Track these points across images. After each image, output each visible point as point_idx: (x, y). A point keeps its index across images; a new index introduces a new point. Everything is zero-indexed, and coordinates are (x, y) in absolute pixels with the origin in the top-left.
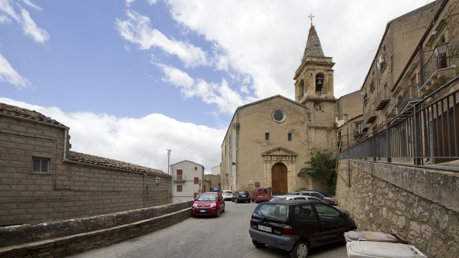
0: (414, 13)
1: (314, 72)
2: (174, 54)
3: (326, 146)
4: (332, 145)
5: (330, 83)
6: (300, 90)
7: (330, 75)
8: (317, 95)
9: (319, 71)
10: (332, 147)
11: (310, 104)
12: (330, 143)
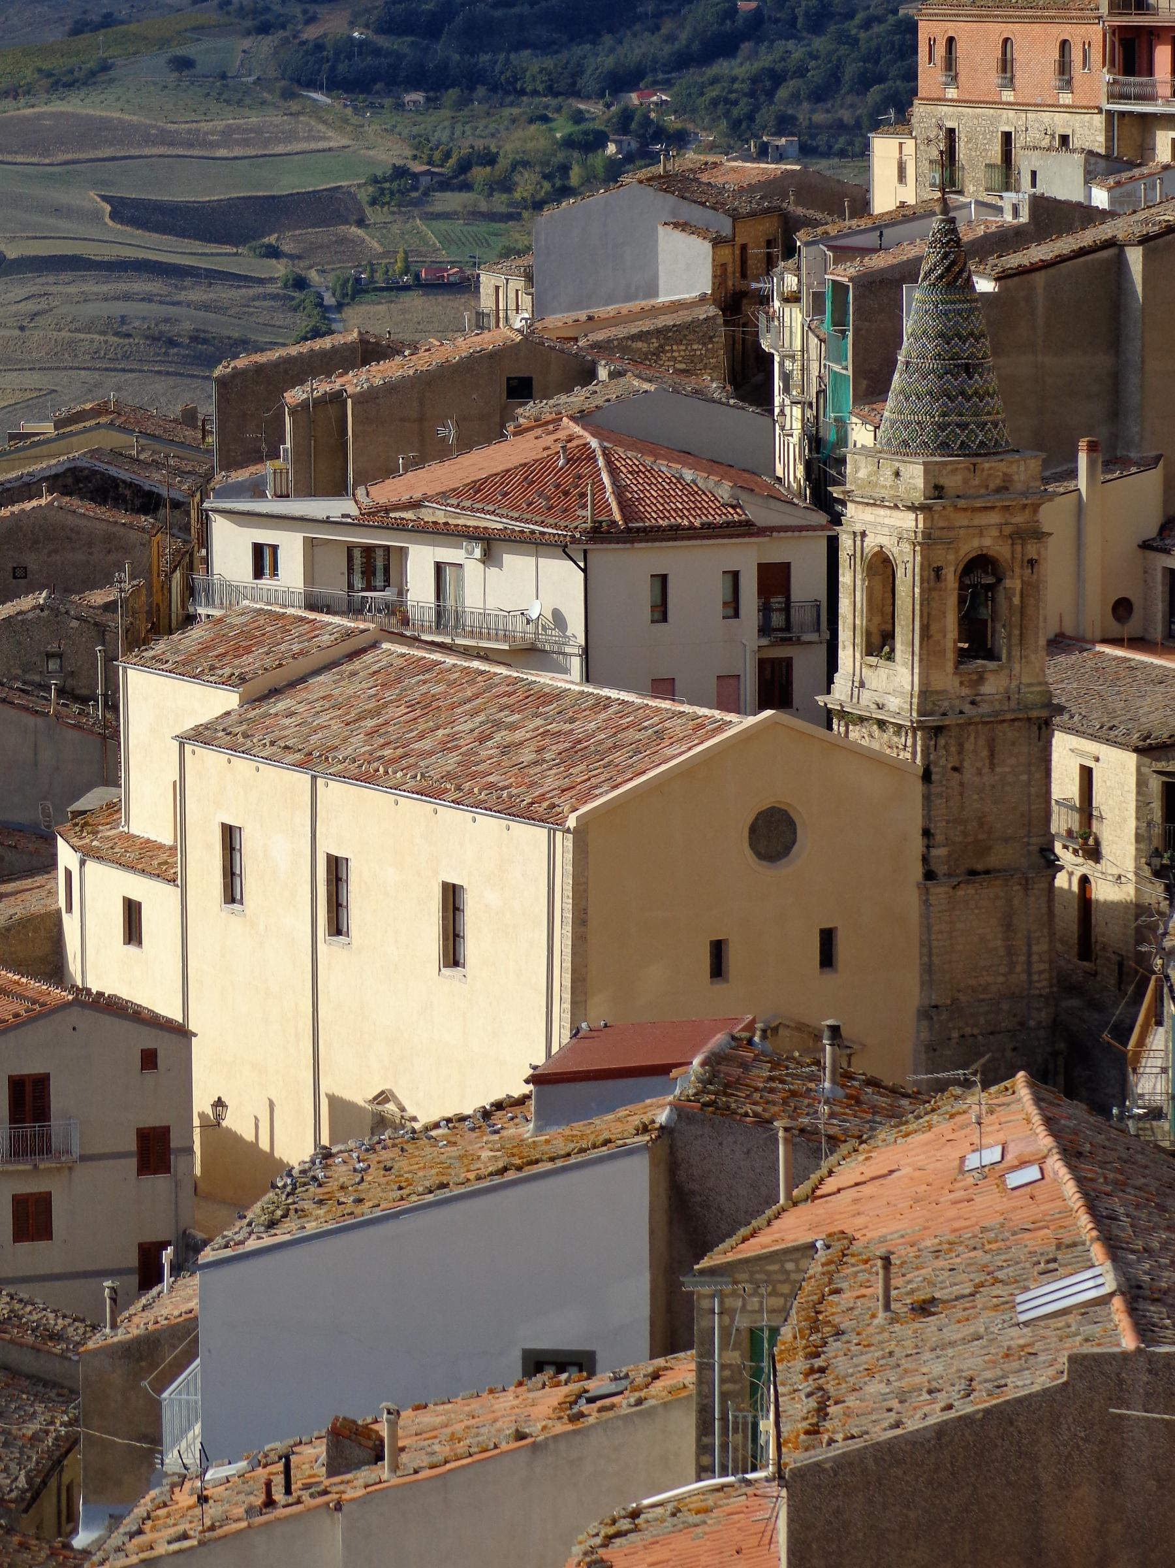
2: (509, 342)
3: (1001, 979)
4: (1029, 973)
7: (1032, 563)
8: (961, 683)
9: (976, 543)
10: (1030, 982)
12: (1022, 959)
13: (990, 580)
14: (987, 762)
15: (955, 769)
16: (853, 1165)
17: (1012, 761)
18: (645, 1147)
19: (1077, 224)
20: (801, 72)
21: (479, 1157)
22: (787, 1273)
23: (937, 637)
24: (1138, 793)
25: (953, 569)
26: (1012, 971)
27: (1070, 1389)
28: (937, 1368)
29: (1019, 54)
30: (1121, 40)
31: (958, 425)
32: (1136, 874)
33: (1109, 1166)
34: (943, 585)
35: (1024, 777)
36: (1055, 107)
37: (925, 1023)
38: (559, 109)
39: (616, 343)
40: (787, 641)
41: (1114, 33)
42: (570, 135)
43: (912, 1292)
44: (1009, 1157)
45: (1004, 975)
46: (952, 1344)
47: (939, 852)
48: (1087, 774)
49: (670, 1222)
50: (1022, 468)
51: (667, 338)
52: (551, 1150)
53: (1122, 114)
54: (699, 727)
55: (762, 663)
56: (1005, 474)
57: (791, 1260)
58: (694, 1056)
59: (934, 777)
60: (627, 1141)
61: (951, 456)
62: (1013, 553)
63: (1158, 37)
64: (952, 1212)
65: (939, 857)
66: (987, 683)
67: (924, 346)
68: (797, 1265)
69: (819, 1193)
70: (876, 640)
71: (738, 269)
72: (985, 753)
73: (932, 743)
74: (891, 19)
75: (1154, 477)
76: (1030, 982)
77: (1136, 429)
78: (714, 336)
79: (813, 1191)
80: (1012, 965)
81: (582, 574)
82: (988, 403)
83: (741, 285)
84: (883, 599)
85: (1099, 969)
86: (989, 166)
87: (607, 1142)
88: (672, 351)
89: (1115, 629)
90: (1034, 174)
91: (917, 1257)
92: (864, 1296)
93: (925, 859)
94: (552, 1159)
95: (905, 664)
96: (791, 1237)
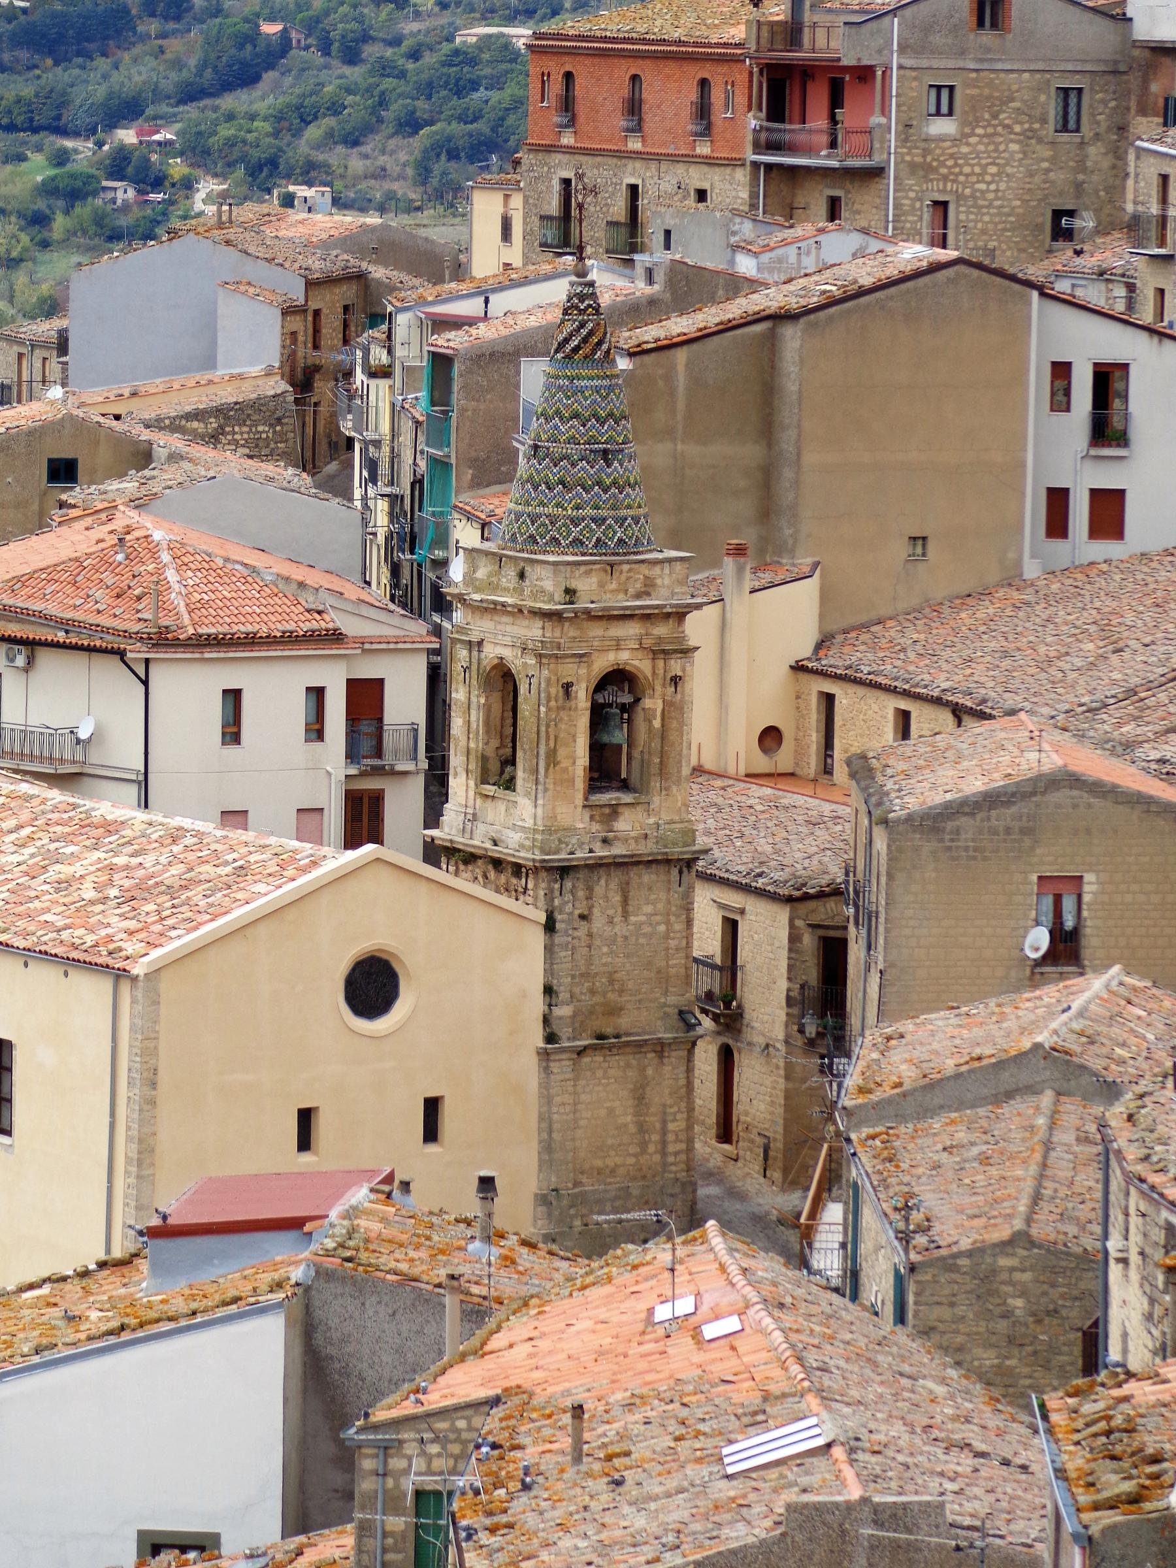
0: (967, 810)
1: (583, 671)
3: (631, 1160)
4: (664, 1154)
5: (673, 736)
6: (488, 708)
7: (676, 680)
8: (592, 818)
10: (665, 1165)
11: (552, 891)
12: (655, 1137)
13: (626, 699)
14: (620, 909)
15: (583, 917)
16: (525, 1319)
17: (649, 909)
18: (279, 1305)
19: (721, 292)
20: (335, 108)
21: (87, 1318)
22: (458, 1431)
23: (565, 763)
24: (790, 950)
25: (584, 685)
26: (644, 1151)
27: (789, 1540)
28: (640, 1522)
29: (648, 95)
30: (769, 80)
31: (593, 520)
32: (786, 1042)
33: (814, 1319)
34: (573, 703)
35: (662, 928)
36: (692, 159)
37: (542, 1209)
38: (39, 149)
39: (167, 422)
40: (378, 771)
41: (761, 72)
42: (53, 179)
43: (604, 1445)
44: (705, 1308)
45: (635, 1155)
46: (656, 1498)
47: (563, 1011)
48: (731, 927)
49: (305, 1391)
50: (667, 571)
51: (227, 418)
52: (171, 1310)
53: (769, 167)
54: (285, 863)
55: (348, 793)
56: (646, 577)
57: (462, 1418)
58: (330, 1207)
59: (558, 926)
60: (261, 1298)
61: (583, 554)
62: (654, 668)
63: (813, 77)
64: (642, 1365)
65: (561, 1018)
66: (621, 818)
67: (556, 427)
68: (469, 1423)
69: (487, 1348)
70: (494, 766)
71: (310, 339)
72: (617, 898)
73: (557, 886)
74: (446, 48)
75: (811, 587)
76: (665, 1165)
77: (788, 532)
78: (284, 416)
79: (483, 1344)
80: (644, 1145)
81: (143, 688)
82: (628, 495)
83: (314, 357)
84: (503, 719)
85: (741, 1153)
86: (610, 224)
87: (235, 1300)
88: (234, 433)
89: (762, 763)
90: (668, 233)
91: (606, 1412)
92: (550, 1451)
93: (546, 1020)
94: (170, 1319)
95: (527, 794)
96: (462, 1393)
